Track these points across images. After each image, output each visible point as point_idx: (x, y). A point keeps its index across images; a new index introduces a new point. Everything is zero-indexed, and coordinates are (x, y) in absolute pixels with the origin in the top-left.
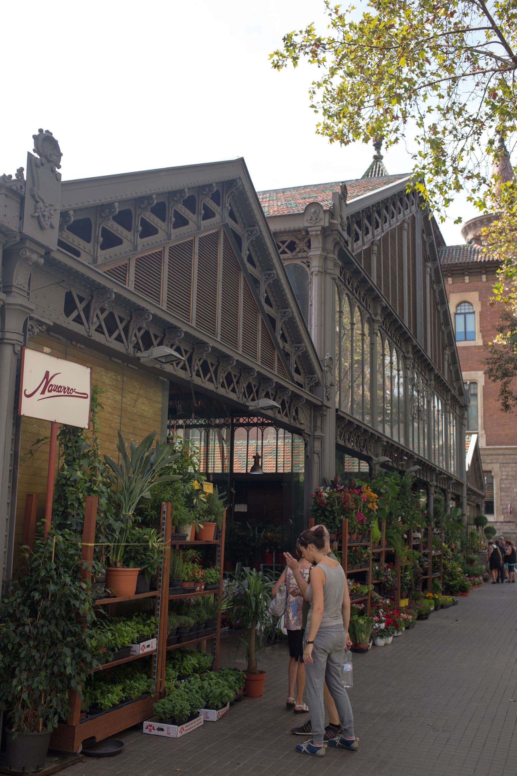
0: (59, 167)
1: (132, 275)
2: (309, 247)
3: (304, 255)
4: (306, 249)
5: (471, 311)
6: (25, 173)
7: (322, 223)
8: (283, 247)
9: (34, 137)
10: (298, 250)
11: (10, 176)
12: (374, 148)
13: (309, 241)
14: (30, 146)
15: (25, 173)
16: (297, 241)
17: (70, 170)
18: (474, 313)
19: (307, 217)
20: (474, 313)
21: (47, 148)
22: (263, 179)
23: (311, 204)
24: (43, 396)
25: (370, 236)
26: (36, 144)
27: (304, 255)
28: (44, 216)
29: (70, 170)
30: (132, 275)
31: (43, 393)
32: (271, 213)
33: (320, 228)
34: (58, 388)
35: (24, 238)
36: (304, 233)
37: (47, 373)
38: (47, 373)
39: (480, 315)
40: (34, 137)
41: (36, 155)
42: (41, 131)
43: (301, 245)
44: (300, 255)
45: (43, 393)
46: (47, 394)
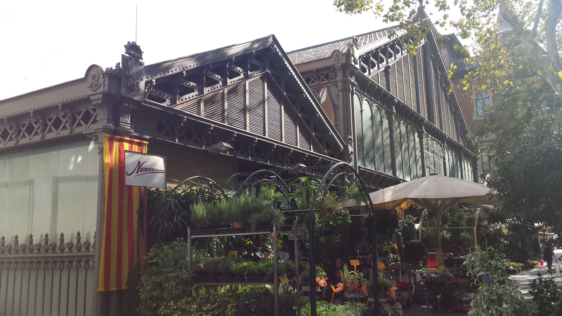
0: (142, 59)
1: (52, 121)
2: (336, 76)
3: (334, 80)
4: (334, 77)
5: (487, 96)
6: (121, 65)
7: (341, 62)
8: (322, 77)
9: (125, 46)
10: (330, 78)
11: (112, 68)
12: (111, 59)
13: (336, 73)
14: (123, 51)
15: (121, 65)
16: (330, 73)
17: (148, 60)
18: (489, 97)
19: (333, 58)
20: (489, 97)
21: (134, 51)
22: (288, 45)
23: (335, 51)
24: (137, 174)
25: (385, 63)
26: (126, 50)
27: (334, 80)
28: (133, 85)
29: (148, 60)
30: (52, 121)
31: (137, 172)
32: (297, 62)
33: (340, 64)
34: (146, 169)
35: (123, 98)
36: (332, 68)
37: (139, 162)
38: (139, 162)
39: (493, 99)
40: (125, 46)
41: (127, 55)
42: (129, 42)
43: (332, 75)
44: (332, 81)
45: (137, 172)
46: (140, 173)
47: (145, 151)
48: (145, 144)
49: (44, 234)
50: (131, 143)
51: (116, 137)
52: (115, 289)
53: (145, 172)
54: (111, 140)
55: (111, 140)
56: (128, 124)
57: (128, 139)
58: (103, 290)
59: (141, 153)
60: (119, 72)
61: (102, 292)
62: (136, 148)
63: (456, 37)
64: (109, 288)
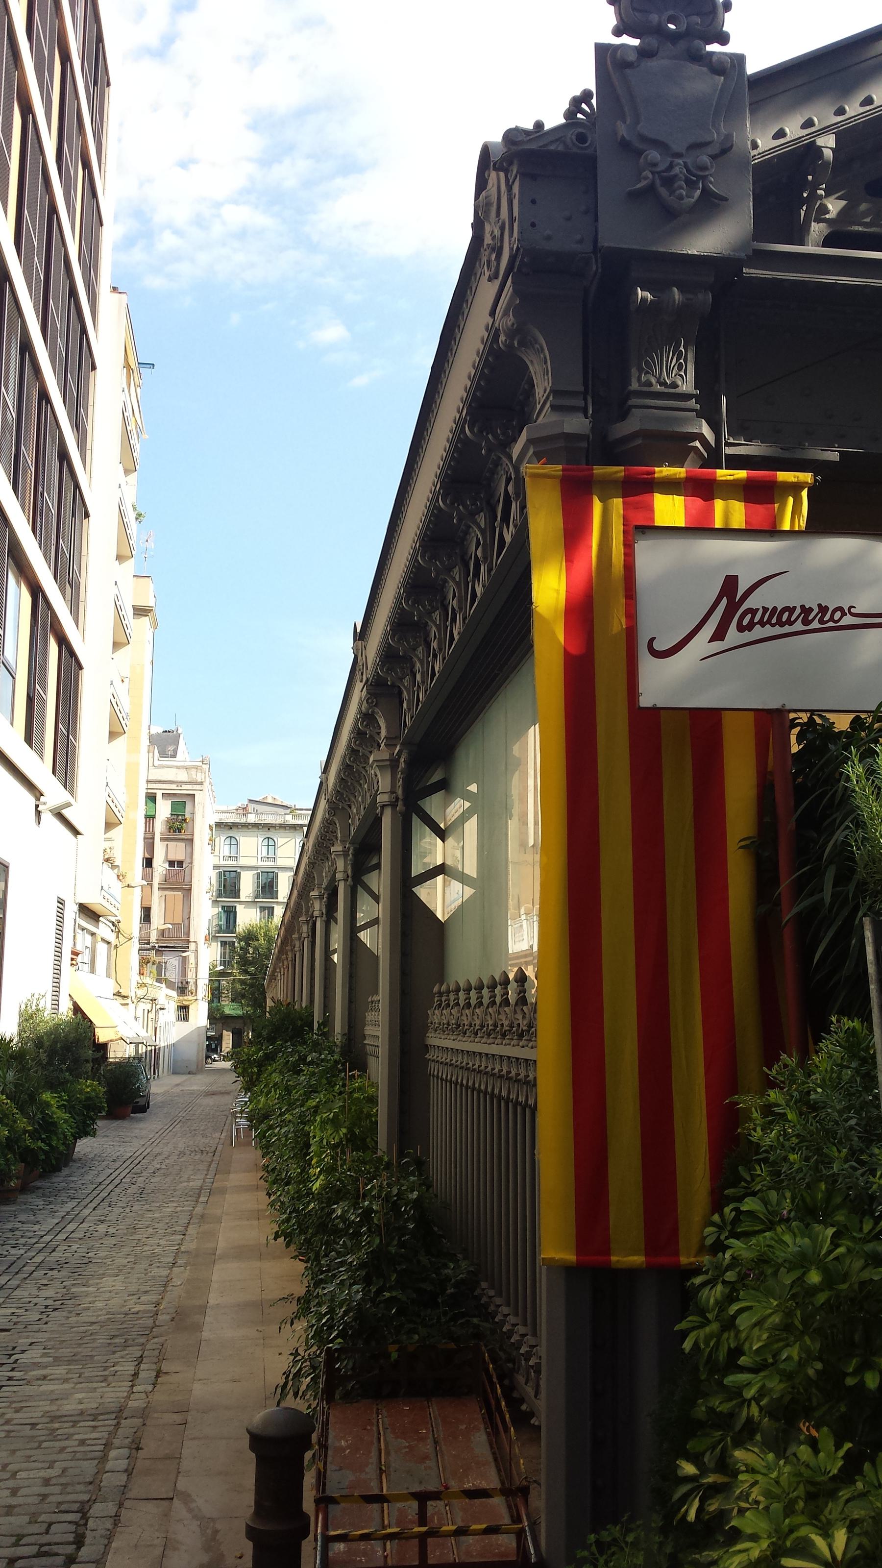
24: (718, 646)
31: (719, 635)
34: (778, 616)
37: (731, 583)
38: (731, 583)
41: (626, 40)
46: (733, 635)
47: (793, 514)
48: (795, 488)
49: (25, 1001)
50: (702, 489)
51: (599, 470)
52: (638, 1260)
53: (769, 631)
54: (576, 495)
55: (576, 495)
56: (686, 397)
57: (680, 472)
58: (570, 1257)
59: (772, 532)
60: (582, 138)
61: (569, 1270)
62: (730, 512)
63: (646, 1248)
64: (607, 1252)
